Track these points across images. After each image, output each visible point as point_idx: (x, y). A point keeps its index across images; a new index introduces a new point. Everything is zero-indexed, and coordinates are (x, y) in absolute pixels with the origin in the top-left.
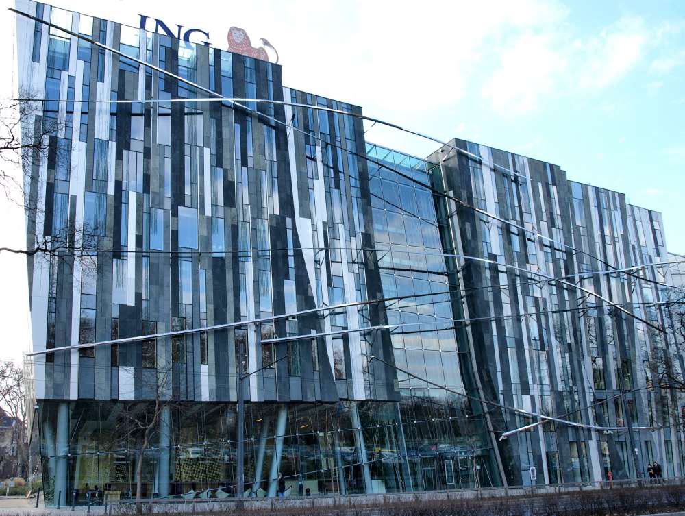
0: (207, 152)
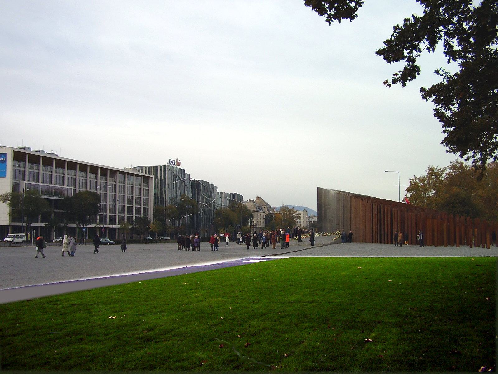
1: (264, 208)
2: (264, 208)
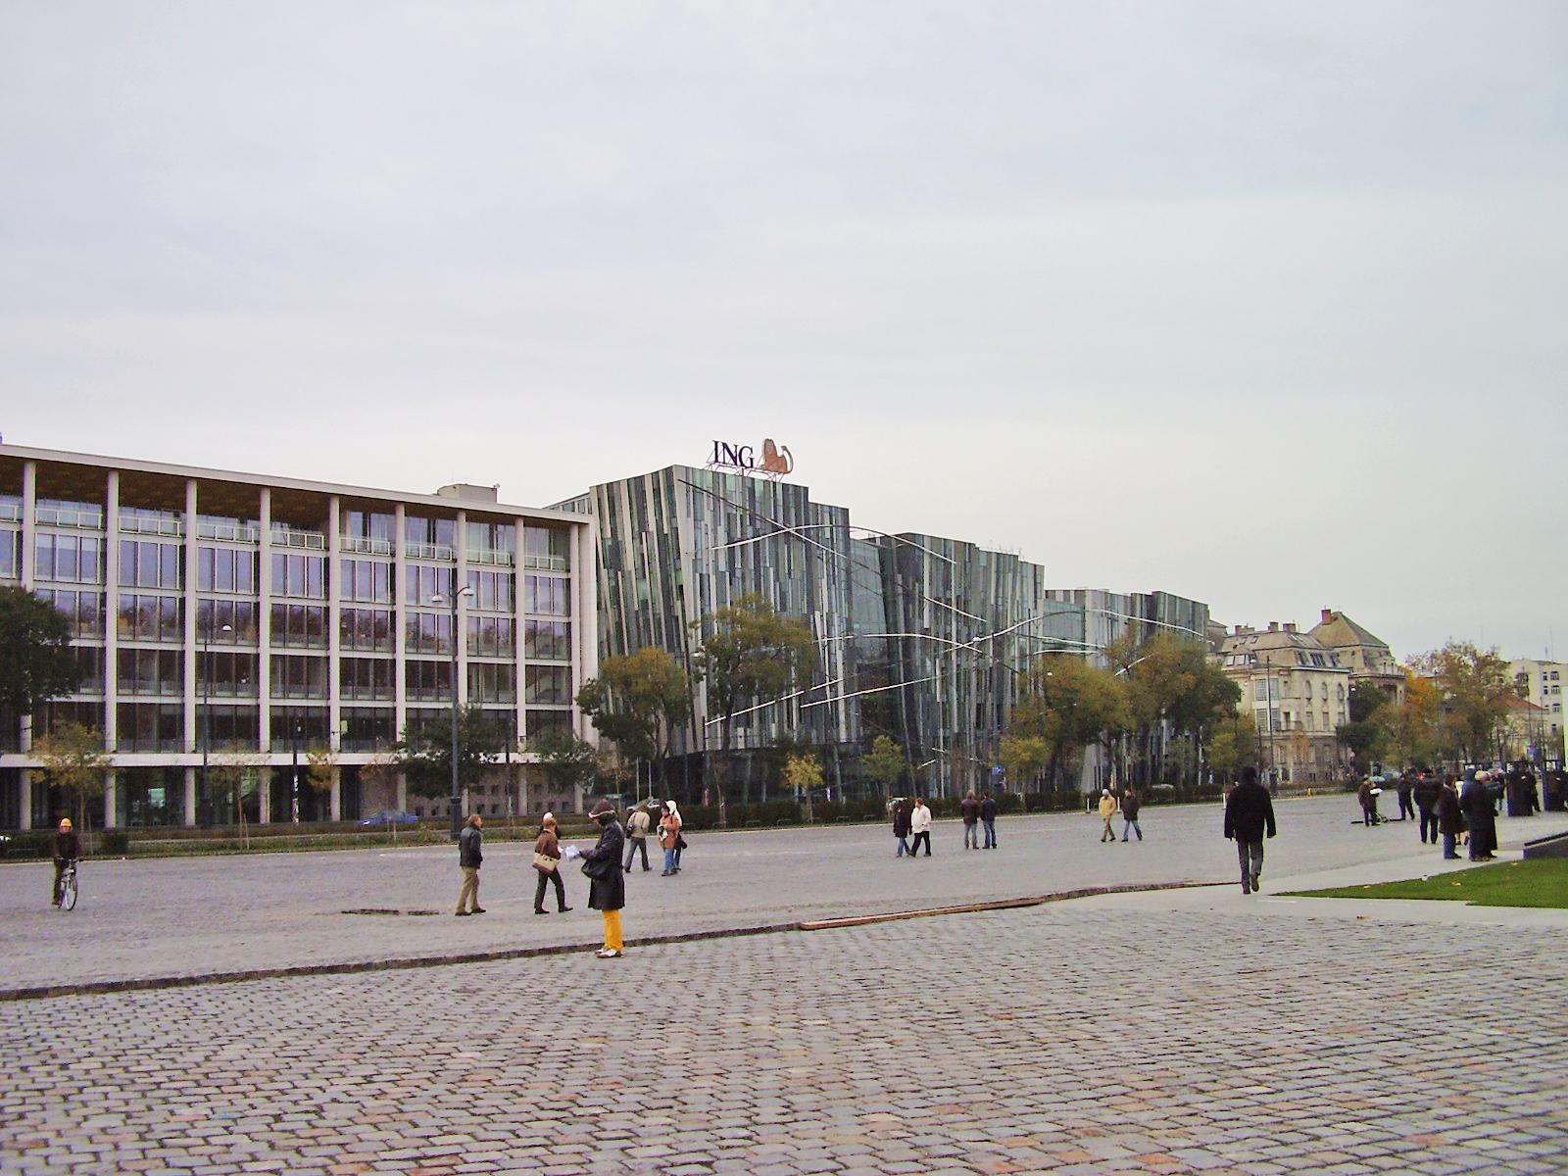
0: (772, 569)
1: (1353, 653)
2: (1353, 653)
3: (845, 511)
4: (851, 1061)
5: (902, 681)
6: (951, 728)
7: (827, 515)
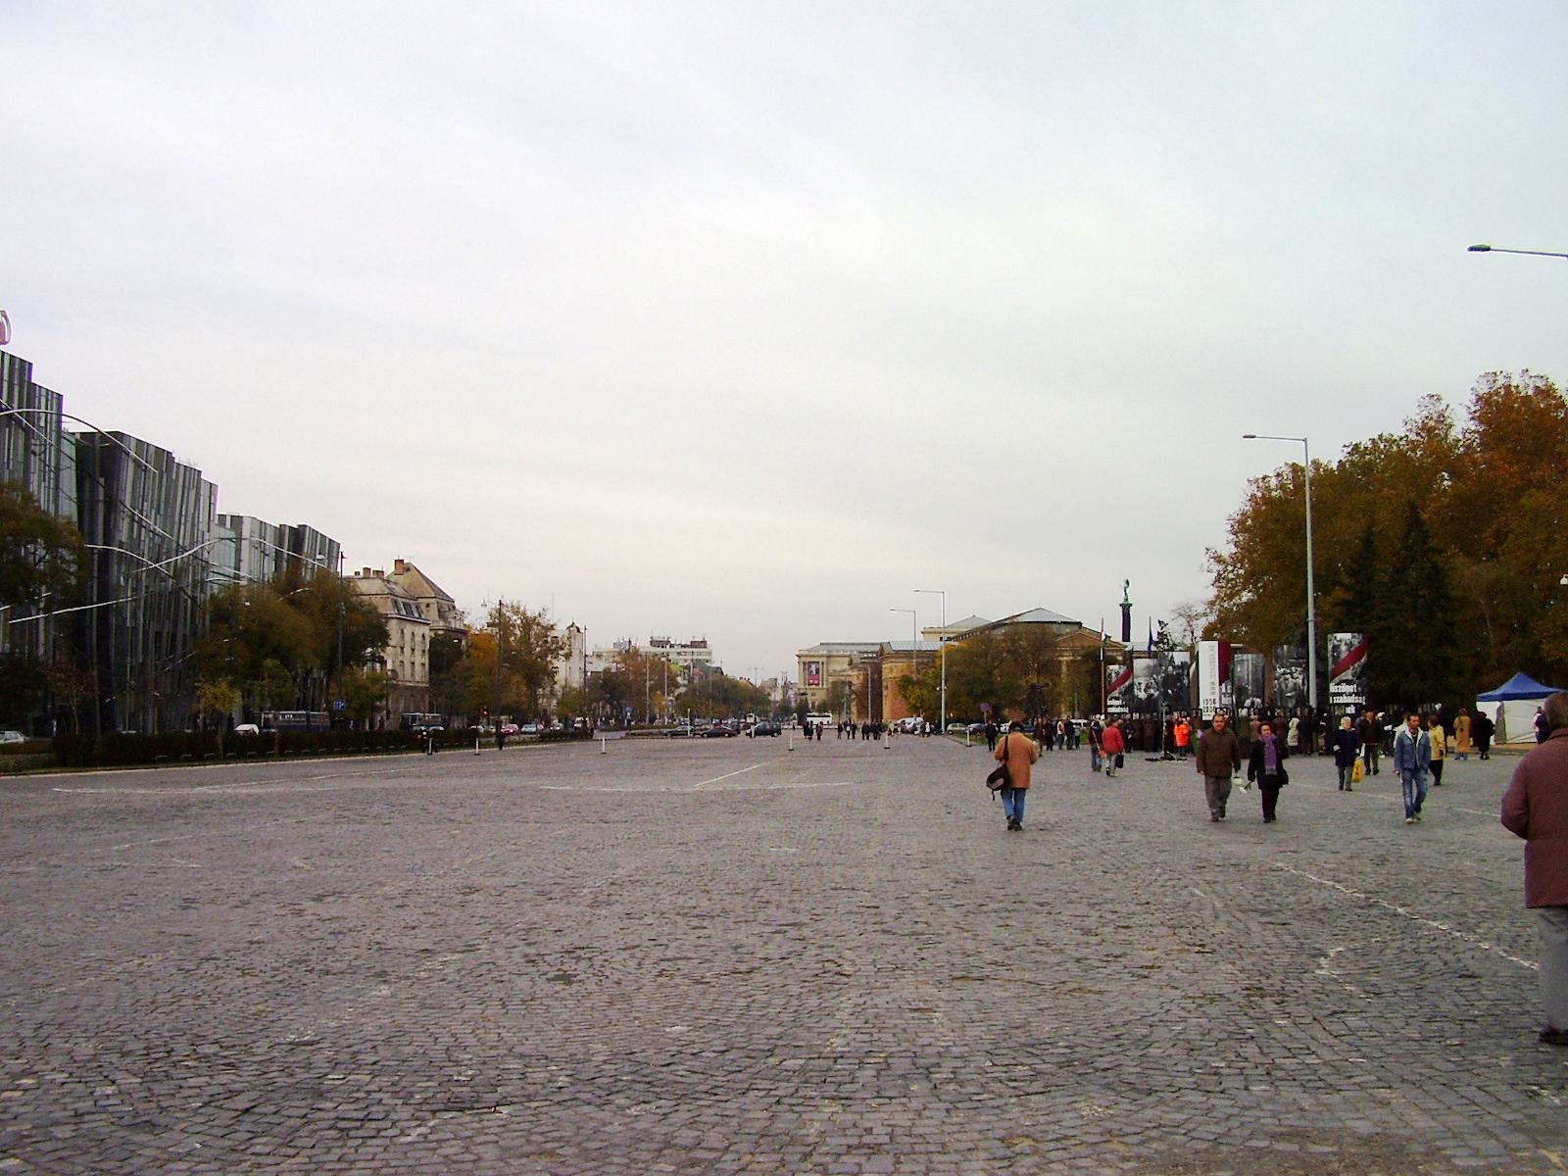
1: (428, 605)
3: (60, 397)
4: (561, 898)
5: (95, 599)
6: (137, 657)
7: (43, 400)
